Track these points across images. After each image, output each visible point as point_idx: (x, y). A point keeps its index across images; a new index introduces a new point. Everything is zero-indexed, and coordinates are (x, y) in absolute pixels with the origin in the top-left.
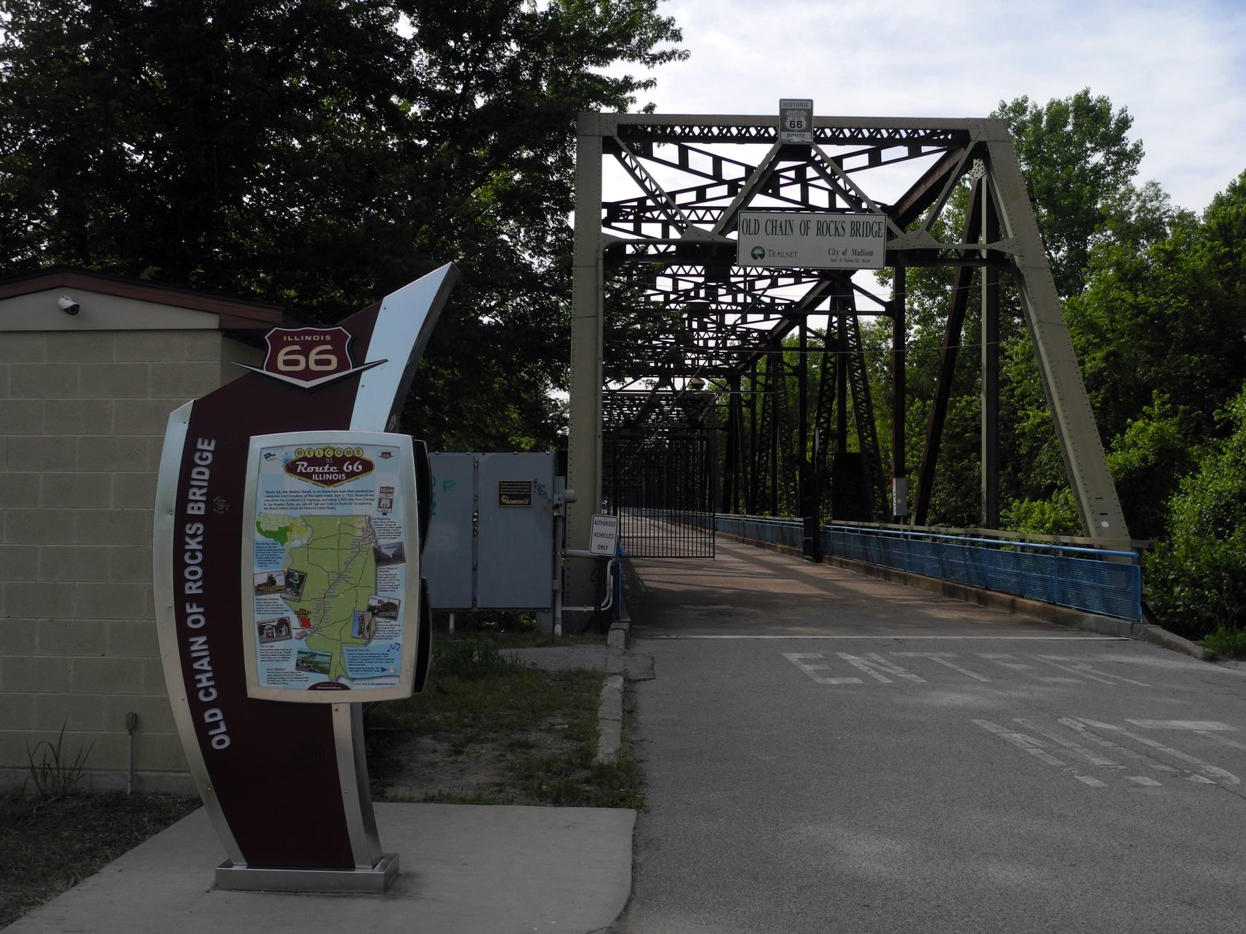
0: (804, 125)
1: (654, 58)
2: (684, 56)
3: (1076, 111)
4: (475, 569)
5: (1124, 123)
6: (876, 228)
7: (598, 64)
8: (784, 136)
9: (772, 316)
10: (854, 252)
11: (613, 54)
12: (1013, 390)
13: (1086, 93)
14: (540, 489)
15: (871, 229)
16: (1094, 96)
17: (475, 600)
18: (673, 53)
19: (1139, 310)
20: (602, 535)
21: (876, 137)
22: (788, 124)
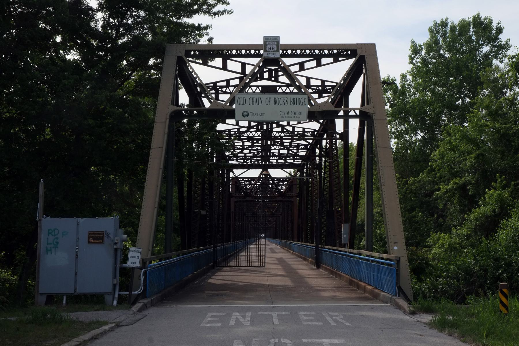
0: (276, 49)
1: (215, 14)
2: (230, 12)
3: (473, 24)
4: (76, 274)
5: (500, 30)
6: (303, 101)
7: (188, 17)
8: (266, 55)
10: (293, 113)
11: (196, 12)
12: (436, 174)
13: (479, 15)
14: (108, 234)
15: (300, 101)
16: (482, 16)
17: (75, 289)
18: (225, 11)
19: (498, 131)
20: (134, 257)
21: (317, 54)
22: (267, 49)
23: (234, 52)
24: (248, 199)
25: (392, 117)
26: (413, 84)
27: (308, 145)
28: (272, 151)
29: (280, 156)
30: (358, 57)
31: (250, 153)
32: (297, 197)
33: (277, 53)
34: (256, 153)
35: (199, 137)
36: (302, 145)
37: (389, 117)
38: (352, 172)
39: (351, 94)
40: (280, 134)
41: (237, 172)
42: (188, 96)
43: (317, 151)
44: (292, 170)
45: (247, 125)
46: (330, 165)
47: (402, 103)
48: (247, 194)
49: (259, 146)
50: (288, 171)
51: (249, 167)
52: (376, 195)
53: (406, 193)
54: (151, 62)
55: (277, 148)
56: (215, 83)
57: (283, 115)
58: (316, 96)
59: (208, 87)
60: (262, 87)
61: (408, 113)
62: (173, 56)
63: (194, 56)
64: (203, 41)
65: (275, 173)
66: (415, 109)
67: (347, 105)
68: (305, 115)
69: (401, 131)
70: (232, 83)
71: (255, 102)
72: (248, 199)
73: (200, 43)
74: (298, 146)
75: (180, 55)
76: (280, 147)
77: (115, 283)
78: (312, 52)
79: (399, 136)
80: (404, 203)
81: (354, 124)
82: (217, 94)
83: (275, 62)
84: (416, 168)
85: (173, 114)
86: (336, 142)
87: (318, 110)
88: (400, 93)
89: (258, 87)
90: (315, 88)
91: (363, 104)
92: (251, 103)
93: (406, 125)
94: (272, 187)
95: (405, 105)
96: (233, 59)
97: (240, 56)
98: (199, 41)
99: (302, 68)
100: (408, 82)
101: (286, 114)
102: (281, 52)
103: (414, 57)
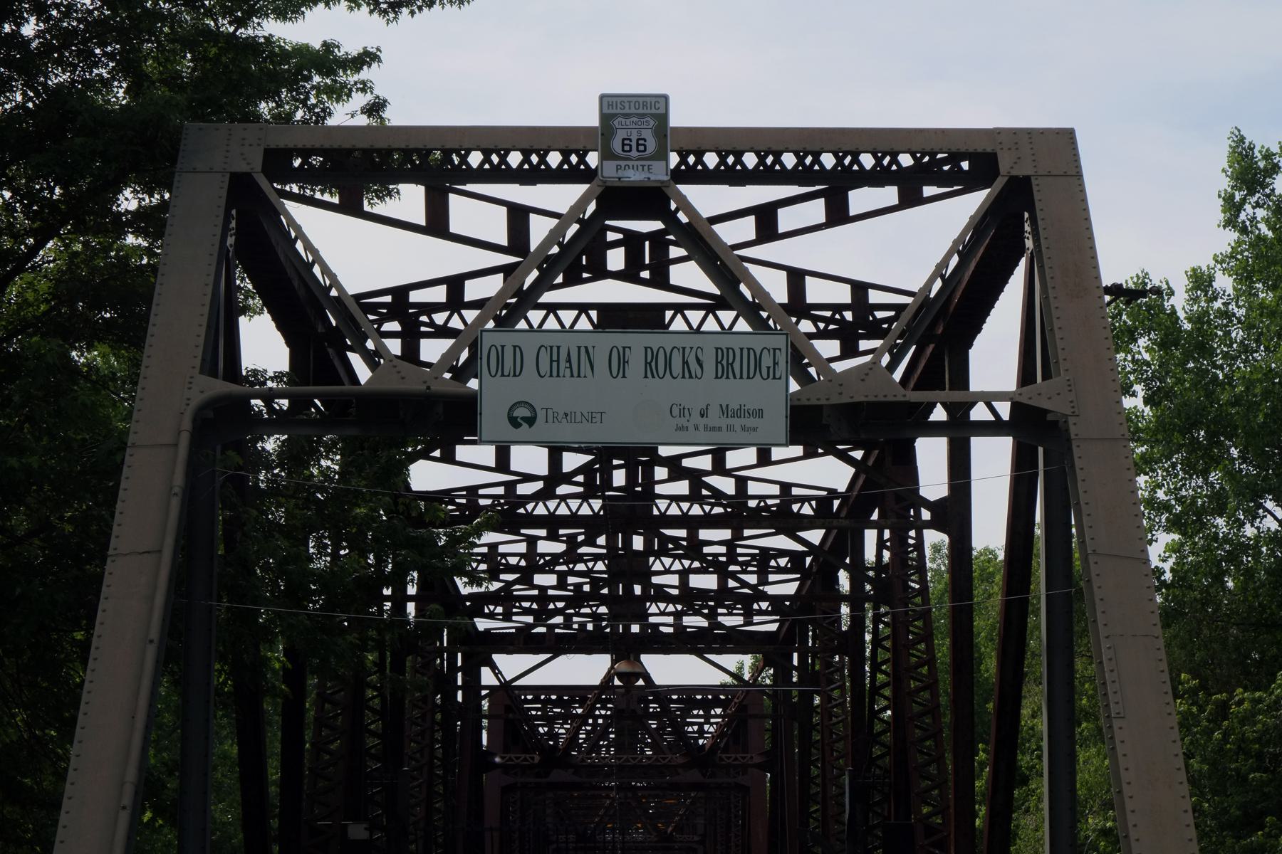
0: (651, 146)
6: (767, 361)
7: (282, 15)
8: (610, 171)
9: (485, 550)
10: (725, 411)
21: (833, 169)
22: (617, 146)
23: (475, 159)
24: (557, 775)
25: (1153, 443)
26: (1241, 312)
27: (804, 554)
28: (655, 580)
29: (690, 599)
30: (1000, 183)
31: (562, 585)
32: (763, 767)
33: (658, 166)
34: (587, 588)
35: (333, 514)
36: (782, 553)
37: (1141, 442)
38: (989, 666)
39: (979, 341)
40: (685, 506)
41: (511, 665)
42: (288, 343)
43: (844, 579)
44: (748, 660)
45: (544, 471)
46: (894, 636)
47: (1195, 385)
48: (555, 757)
49: (596, 558)
50: (730, 661)
51: (556, 646)
52: (1089, 762)
53: (1220, 750)
54: (129, 201)
55: (677, 566)
56: (400, 293)
57: (682, 421)
58: (828, 348)
59: (373, 308)
60: (602, 308)
61: (1221, 428)
62: (211, 171)
63: (307, 176)
64: (346, 114)
65: (667, 670)
66: (1253, 407)
67: (961, 377)
68: (778, 421)
69: (1194, 498)
70: (474, 290)
71: (563, 363)
72: (557, 775)
73: (330, 122)
74: (764, 559)
75: (243, 168)
76: (687, 563)
78: (808, 160)
79: (1187, 521)
80: (1215, 793)
81: (993, 460)
82: (411, 337)
83: (651, 200)
84: (1262, 653)
85: (211, 414)
86: (920, 538)
87: (835, 400)
88: (1187, 343)
89: (583, 308)
90: (828, 314)
91: (1026, 375)
92: (545, 367)
93: (1214, 476)
94: (661, 727)
95: (1210, 395)
96: (470, 187)
97: (502, 174)
98: (327, 113)
99: (766, 219)
100: (1218, 304)
101: (696, 414)
102: (674, 159)
103: (1244, 201)
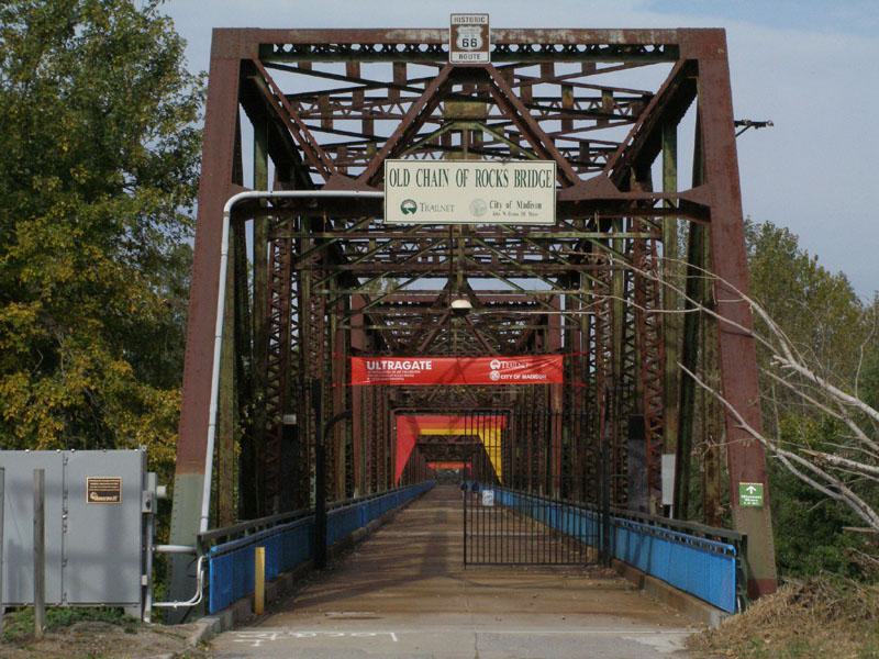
0: (480, 43)
6: (543, 177)
15: (539, 179)
22: (459, 43)
30: (681, 63)
77: (145, 583)
101: (504, 207)
